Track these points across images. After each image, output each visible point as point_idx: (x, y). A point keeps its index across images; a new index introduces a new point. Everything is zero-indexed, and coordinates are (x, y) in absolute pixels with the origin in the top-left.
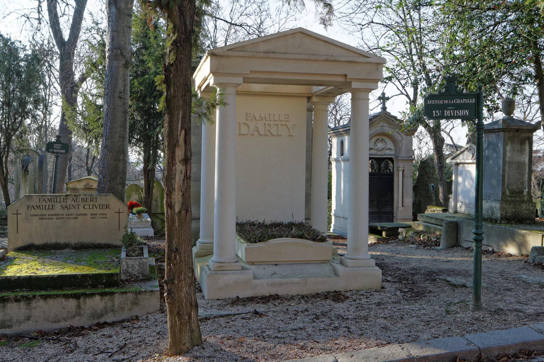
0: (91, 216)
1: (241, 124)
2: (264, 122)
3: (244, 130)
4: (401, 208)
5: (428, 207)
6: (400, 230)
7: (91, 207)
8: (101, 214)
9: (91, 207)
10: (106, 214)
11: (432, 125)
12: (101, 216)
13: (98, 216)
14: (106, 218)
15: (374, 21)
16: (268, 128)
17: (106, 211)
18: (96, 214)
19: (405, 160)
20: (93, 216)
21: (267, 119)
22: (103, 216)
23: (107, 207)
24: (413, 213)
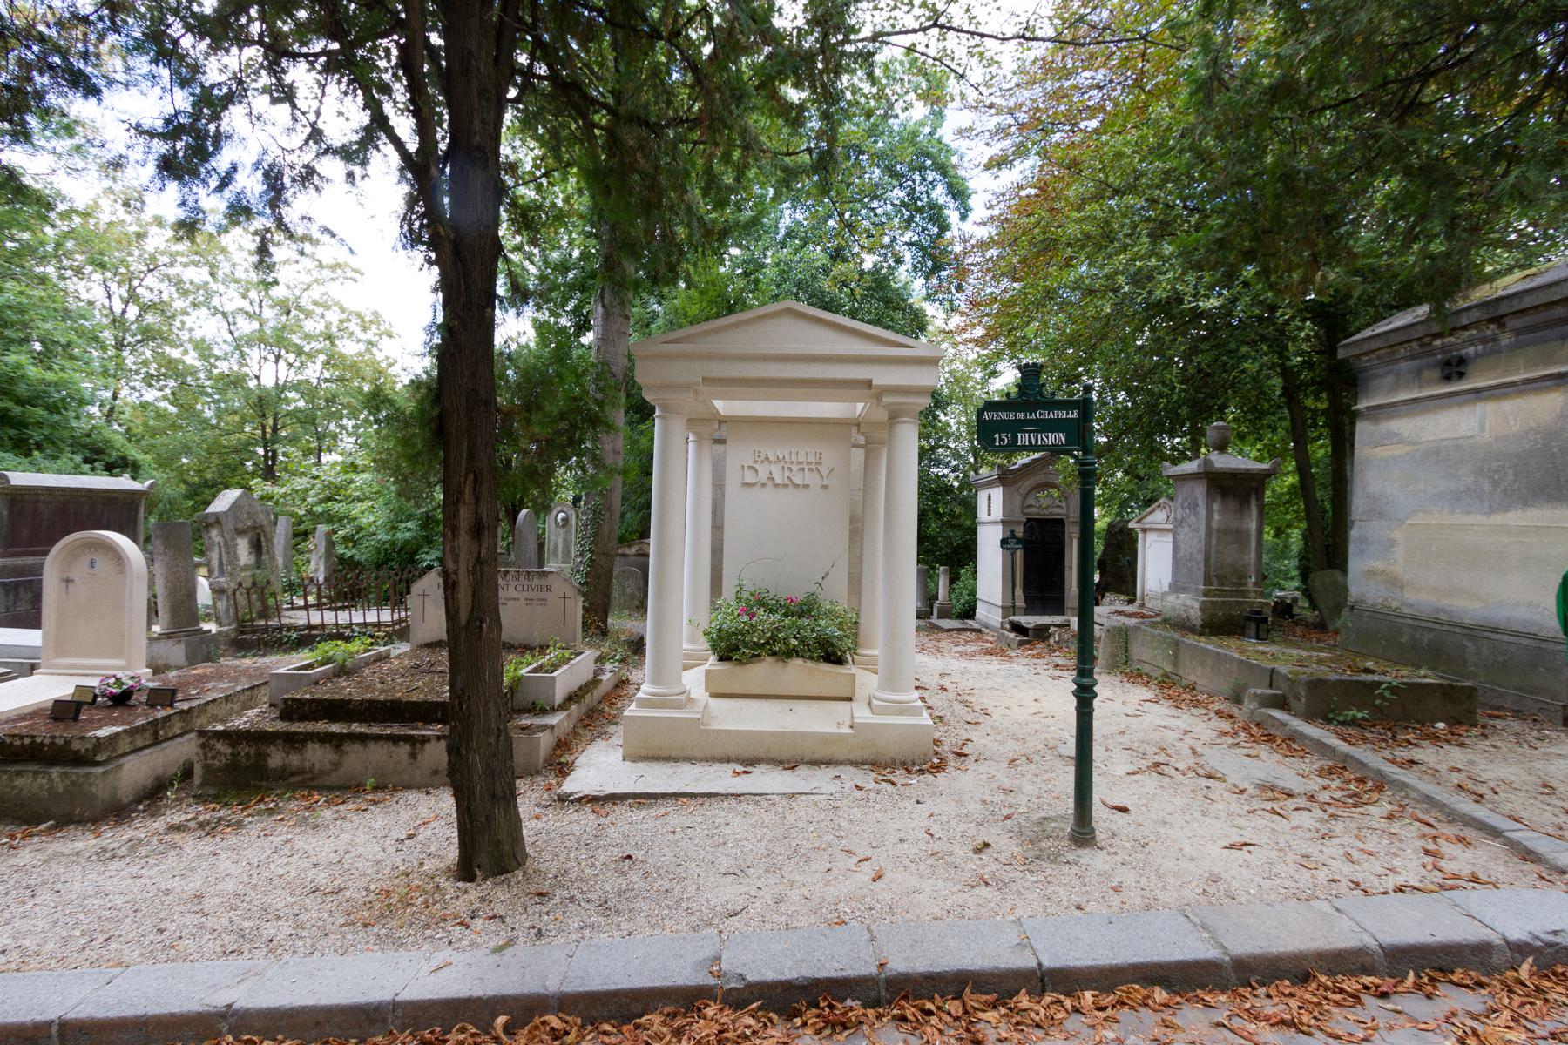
3: (750, 477)
6: (1052, 629)
16: (787, 474)
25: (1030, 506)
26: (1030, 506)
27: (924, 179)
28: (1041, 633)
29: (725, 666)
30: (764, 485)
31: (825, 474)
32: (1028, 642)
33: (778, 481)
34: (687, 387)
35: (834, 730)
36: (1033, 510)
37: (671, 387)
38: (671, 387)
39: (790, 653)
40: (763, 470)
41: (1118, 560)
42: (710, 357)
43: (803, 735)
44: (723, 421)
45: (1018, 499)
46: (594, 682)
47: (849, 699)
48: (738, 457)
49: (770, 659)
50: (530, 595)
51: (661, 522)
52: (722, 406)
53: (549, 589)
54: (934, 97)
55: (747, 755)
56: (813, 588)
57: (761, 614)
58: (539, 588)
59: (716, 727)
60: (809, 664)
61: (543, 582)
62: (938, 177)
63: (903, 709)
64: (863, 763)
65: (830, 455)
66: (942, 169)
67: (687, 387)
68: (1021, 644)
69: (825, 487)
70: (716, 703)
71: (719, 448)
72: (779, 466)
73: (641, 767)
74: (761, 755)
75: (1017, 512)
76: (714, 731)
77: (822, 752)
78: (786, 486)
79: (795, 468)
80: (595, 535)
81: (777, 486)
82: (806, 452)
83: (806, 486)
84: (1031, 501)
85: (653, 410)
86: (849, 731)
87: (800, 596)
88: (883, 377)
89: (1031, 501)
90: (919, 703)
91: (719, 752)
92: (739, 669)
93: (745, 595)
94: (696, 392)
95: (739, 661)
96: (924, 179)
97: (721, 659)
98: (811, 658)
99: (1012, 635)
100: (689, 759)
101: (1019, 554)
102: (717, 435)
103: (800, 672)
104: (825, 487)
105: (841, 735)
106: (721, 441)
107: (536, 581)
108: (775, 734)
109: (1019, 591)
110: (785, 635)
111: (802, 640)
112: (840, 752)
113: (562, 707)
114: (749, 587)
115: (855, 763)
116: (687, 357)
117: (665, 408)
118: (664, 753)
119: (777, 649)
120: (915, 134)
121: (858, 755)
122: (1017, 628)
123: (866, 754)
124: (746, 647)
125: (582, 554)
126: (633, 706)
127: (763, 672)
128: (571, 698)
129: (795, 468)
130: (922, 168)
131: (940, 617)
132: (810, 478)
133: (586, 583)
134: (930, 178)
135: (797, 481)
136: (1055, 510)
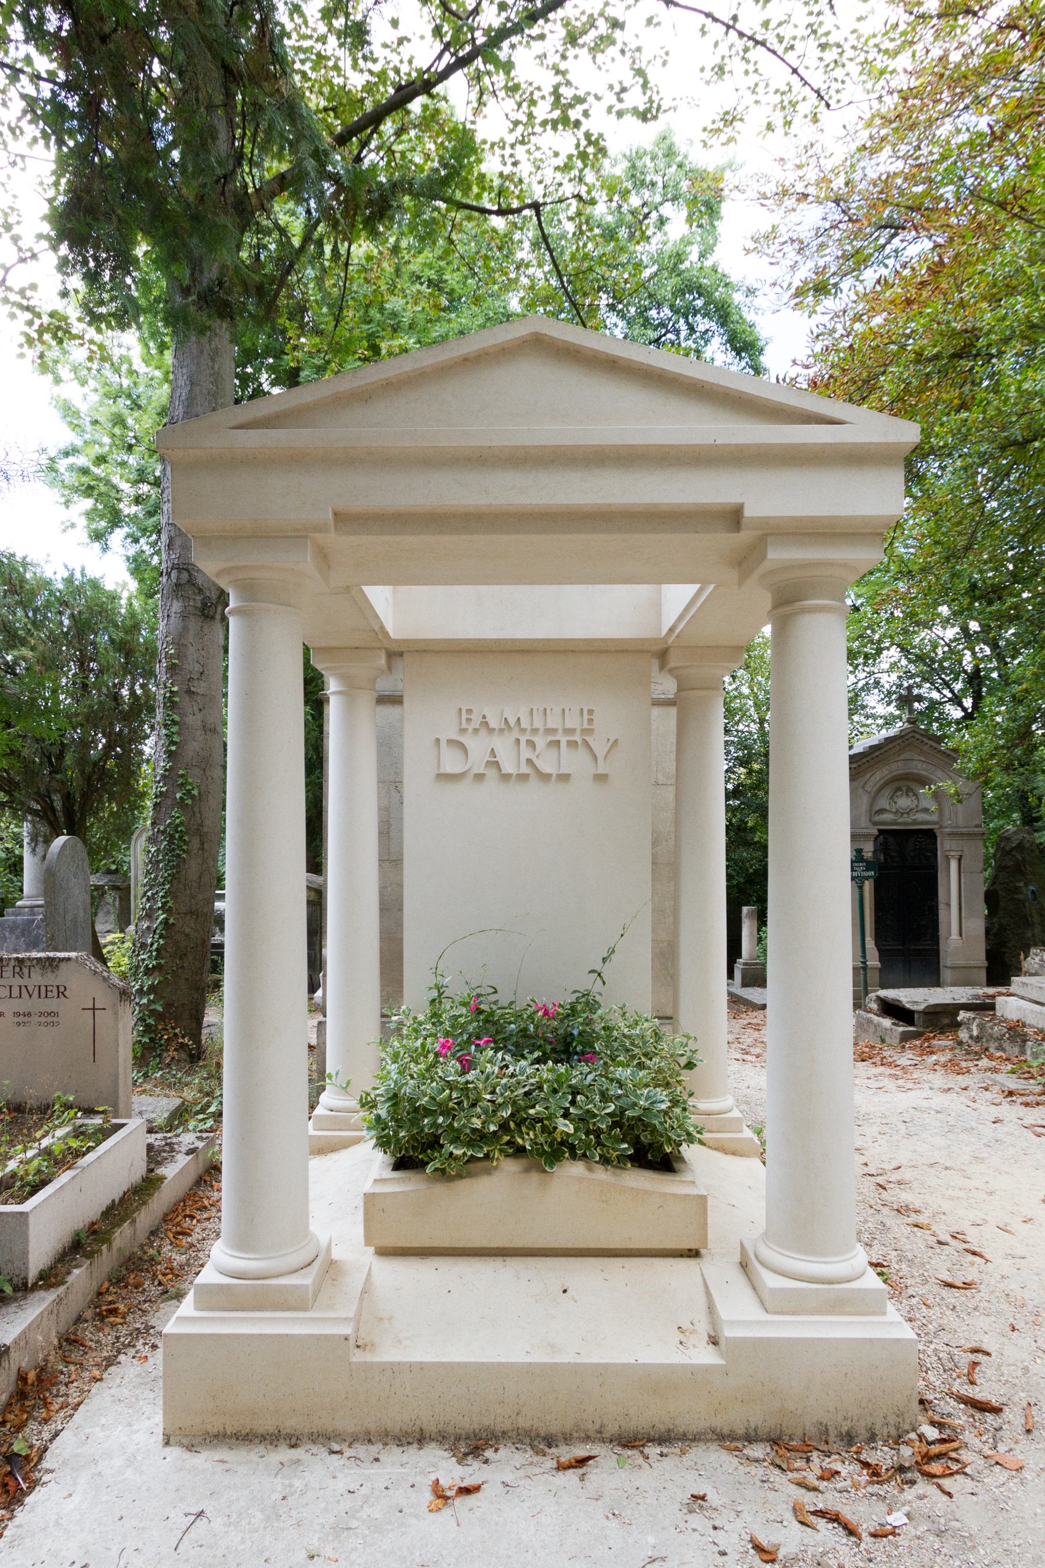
0: (16, 1020)
1: (443, 744)
2: (516, 734)
3: (452, 763)
4: (954, 935)
5: (1033, 951)
6: (962, 1015)
7: (15, 992)
8: (41, 1014)
9: (15, 992)
10: (56, 1014)
11: (916, 705)
12: (43, 1019)
13: (35, 1019)
14: (58, 1023)
15: (724, 29)
16: (526, 753)
17: (53, 1004)
18: (29, 1014)
19: (962, 834)
20: (21, 1019)
21: (525, 724)
22: (49, 1019)
23: (61, 992)
24: (988, 952)
25: (882, 811)
26: (882, 811)
27: (692, 329)
28: (942, 1020)
29: (408, 1184)
30: (479, 777)
31: (600, 752)
32: (917, 1035)
33: (508, 768)
34: (296, 536)
35: (674, 1357)
36: (886, 817)
37: (262, 536)
38: (262, 536)
39: (557, 1151)
40: (478, 747)
41: (1017, 890)
42: (350, 460)
43: (602, 1371)
44: (396, 653)
45: (865, 800)
46: (149, 1184)
47: (694, 1254)
48: (428, 722)
49: (510, 1166)
50: (23, 1004)
51: (249, 865)
52: (395, 608)
53: (61, 992)
54: (706, 207)
55: (467, 1424)
56: (586, 983)
57: (490, 1061)
58: (43, 992)
59: (388, 1354)
60: (602, 1174)
61: (50, 979)
62: (713, 326)
63: (839, 1301)
64: (751, 1438)
65: (612, 716)
66: (723, 314)
67: (296, 536)
68: (905, 1037)
69: (601, 778)
70: (393, 1275)
71: (390, 712)
72: (509, 739)
73: (205, 1460)
74: (503, 1424)
75: (864, 822)
76: (394, 1369)
77: (648, 1414)
78: (523, 778)
79: (540, 741)
80: (173, 878)
81: (506, 777)
82: (560, 708)
83: (564, 778)
84: (883, 803)
85: (223, 598)
86: (705, 1356)
87: (558, 994)
88: (768, 498)
89: (883, 803)
90: (872, 1281)
91: (398, 1417)
92: (440, 1189)
93: (449, 1010)
94: (324, 557)
95: (442, 1174)
96: (692, 329)
97: (401, 1164)
98: (605, 1161)
99: (887, 1022)
100: (327, 1439)
101: (868, 886)
102: (385, 685)
103: (581, 1195)
104: (601, 778)
105: (694, 1372)
106: (393, 700)
107: (37, 978)
108: (530, 1371)
109: (870, 943)
110: (548, 1103)
111: (583, 1120)
112: (692, 1414)
113: (50, 1278)
114: (457, 990)
115: (730, 1439)
116: (296, 461)
117: (250, 590)
118: (266, 1424)
119: (530, 1141)
120: (679, 257)
121: (736, 1419)
122: (891, 1009)
123: (757, 1417)
124: (456, 1141)
125: (149, 915)
126: (187, 1306)
127: (495, 1196)
128: (78, 1247)
129: (540, 741)
130: (687, 312)
131: (745, 985)
132: (574, 762)
133: (158, 968)
134: (701, 328)
135: (546, 768)
136: (921, 817)
